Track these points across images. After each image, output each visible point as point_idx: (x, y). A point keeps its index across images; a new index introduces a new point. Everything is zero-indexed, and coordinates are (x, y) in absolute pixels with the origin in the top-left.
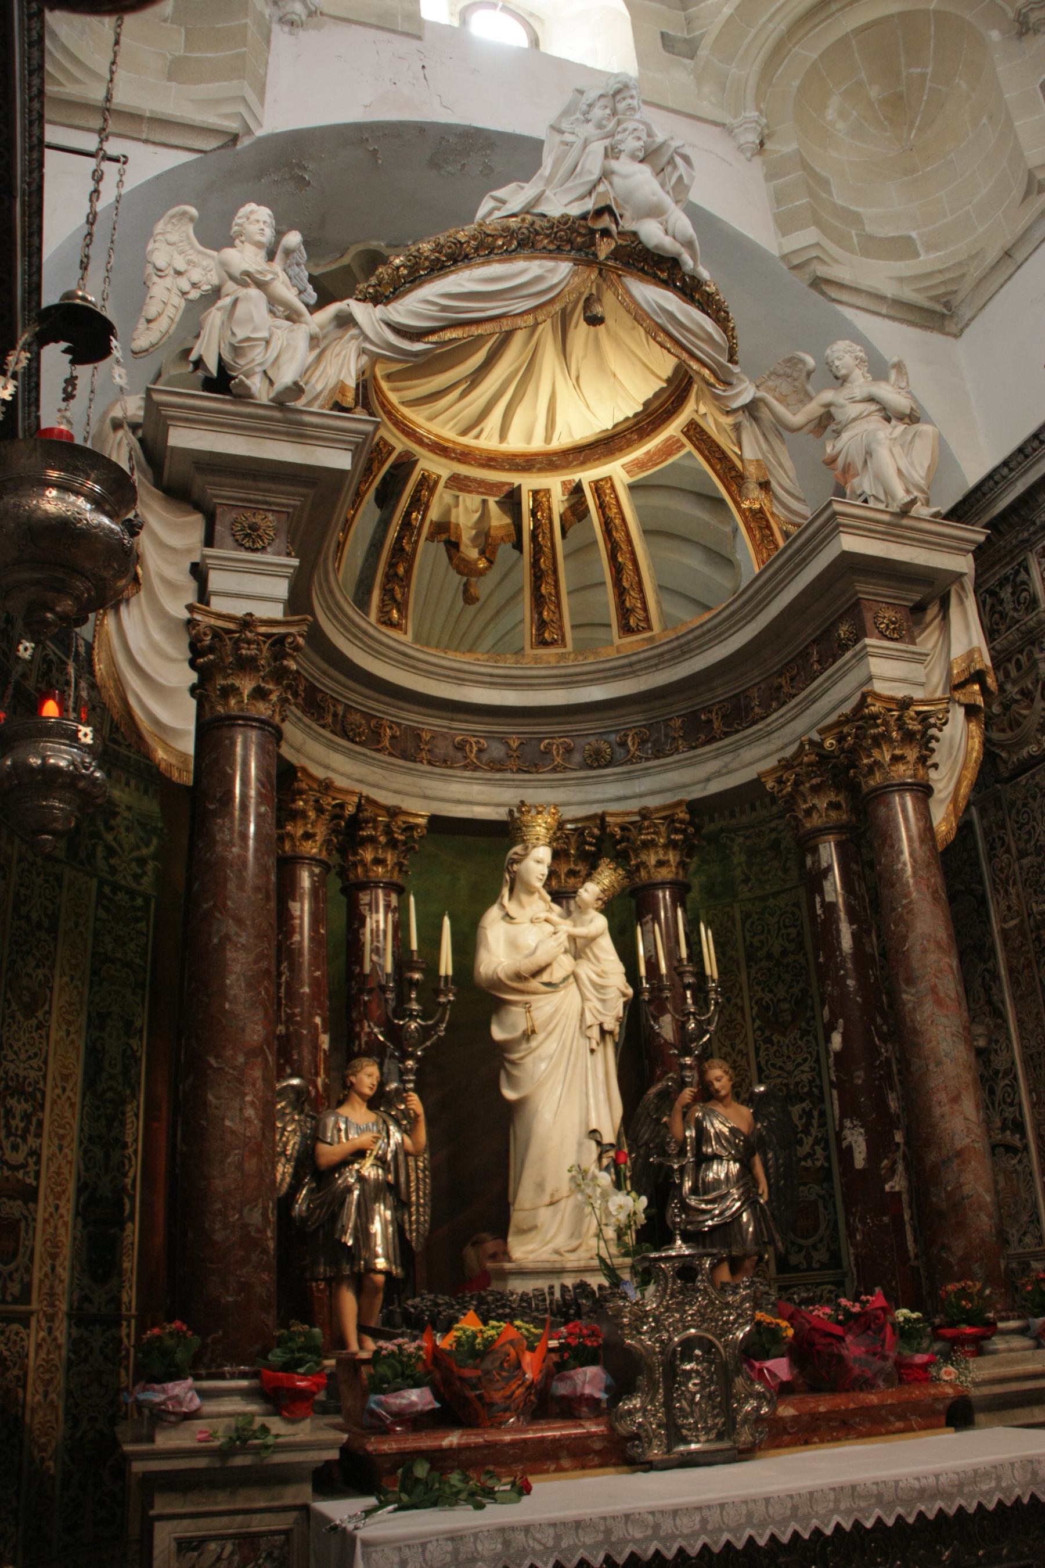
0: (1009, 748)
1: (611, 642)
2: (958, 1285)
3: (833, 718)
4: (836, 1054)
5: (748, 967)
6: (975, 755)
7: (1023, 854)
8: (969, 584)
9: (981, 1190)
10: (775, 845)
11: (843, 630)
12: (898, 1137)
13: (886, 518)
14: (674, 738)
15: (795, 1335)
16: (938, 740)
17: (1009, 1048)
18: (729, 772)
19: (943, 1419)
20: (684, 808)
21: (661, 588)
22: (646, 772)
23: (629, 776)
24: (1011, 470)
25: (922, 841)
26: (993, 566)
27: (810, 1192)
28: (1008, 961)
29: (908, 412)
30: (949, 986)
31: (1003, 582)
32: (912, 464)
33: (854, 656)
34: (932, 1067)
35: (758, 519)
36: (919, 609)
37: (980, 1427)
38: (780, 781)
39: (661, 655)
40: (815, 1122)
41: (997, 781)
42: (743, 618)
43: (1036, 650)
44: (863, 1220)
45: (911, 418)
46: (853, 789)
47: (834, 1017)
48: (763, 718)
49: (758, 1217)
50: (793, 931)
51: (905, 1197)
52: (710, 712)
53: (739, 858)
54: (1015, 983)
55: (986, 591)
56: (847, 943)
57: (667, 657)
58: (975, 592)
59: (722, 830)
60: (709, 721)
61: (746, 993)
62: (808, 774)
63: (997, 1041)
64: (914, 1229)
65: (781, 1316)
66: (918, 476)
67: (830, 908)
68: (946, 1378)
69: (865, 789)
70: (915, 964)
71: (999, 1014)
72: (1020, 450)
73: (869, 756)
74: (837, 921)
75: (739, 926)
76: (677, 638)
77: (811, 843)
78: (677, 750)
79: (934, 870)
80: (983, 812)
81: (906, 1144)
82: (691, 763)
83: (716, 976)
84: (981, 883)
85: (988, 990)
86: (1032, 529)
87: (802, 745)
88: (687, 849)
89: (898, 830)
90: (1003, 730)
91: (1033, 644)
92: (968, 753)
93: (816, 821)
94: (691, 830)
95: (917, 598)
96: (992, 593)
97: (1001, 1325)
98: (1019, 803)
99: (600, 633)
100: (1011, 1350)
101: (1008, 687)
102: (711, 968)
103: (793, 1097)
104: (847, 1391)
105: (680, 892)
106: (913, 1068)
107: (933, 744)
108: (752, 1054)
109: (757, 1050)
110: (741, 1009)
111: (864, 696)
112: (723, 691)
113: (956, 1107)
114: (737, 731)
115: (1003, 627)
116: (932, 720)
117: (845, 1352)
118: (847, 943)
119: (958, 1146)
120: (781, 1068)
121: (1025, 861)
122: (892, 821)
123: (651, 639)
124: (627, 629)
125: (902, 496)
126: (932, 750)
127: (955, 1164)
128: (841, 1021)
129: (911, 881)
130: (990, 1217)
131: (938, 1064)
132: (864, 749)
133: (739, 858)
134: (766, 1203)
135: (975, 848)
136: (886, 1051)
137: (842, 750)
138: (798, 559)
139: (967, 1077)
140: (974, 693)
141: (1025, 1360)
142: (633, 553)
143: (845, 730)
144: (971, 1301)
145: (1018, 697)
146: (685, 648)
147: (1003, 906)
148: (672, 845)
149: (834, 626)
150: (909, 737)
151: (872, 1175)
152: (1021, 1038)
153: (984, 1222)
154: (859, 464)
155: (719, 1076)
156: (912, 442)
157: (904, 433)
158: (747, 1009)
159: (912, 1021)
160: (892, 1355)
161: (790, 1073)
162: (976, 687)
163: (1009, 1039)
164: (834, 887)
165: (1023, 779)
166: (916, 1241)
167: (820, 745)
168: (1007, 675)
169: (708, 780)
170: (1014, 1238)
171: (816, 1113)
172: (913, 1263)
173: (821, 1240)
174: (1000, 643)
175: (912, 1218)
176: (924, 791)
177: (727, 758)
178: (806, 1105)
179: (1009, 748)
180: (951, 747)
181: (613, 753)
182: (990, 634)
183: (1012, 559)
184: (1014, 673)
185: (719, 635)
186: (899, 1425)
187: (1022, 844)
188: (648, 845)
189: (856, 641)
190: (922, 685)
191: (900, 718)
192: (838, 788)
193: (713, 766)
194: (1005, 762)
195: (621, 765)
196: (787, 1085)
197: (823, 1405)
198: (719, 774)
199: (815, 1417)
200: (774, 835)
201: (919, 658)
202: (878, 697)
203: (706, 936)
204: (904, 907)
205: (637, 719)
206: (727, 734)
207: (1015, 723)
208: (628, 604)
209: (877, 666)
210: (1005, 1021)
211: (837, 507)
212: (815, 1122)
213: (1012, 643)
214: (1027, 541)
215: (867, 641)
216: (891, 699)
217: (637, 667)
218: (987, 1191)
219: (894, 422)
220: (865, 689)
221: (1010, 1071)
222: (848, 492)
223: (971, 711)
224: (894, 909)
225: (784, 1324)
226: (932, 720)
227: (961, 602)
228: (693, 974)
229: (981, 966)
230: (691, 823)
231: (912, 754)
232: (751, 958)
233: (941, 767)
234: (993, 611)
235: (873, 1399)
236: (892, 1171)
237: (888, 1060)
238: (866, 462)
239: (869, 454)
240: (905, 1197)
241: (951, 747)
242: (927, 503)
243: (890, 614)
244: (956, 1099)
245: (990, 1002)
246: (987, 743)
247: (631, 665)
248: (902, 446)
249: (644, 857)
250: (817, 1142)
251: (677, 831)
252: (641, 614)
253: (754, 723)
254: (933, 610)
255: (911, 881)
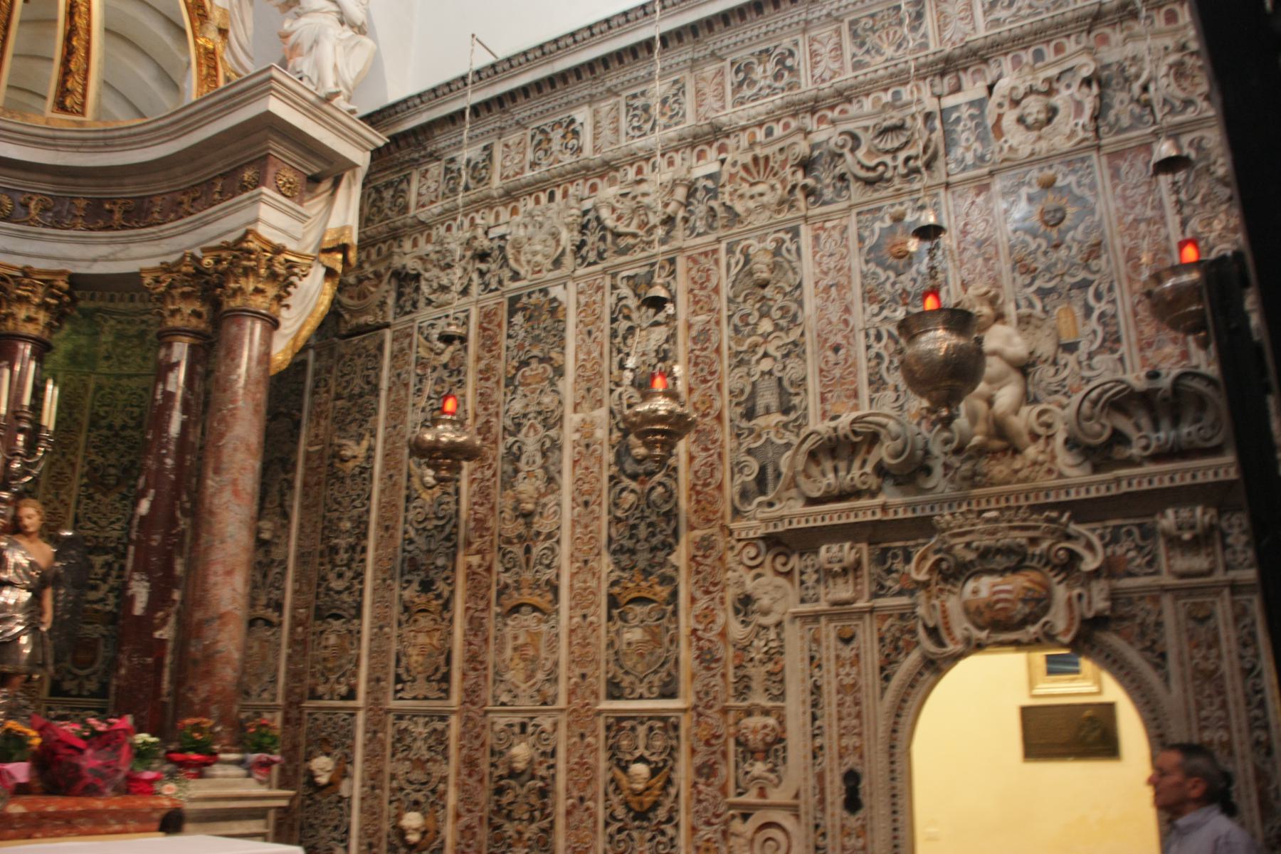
0: (353, 313)
1: (41, 113)
2: (196, 720)
3: (216, 243)
4: (142, 518)
5: (89, 431)
6: (322, 308)
7: (338, 397)
8: (361, 174)
9: (232, 648)
10: (142, 334)
11: (248, 175)
12: (177, 595)
13: (312, 98)
14: (75, 216)
15: (41, 745)
16: (296, 287)
17: (287, 545)
18: (115, 260)
19: (156, 825)
20: (65, 278)
21: (106, 84)
22: (40, 237)
23: (23, 235)
24: (422, 102)
25: (260, 362)
26: (386, 169)
27: (95, 631)
28: (305, 476)
29: (359, 23)
30: (248, 481)
31: (388, 185)
32: (347, 65)
33: (250, 198)
34: (217, 543)
35: (209, 56)
36: (315, 180)
37: (189, 833)
38: (157, 281)
39: (85, 140)
40: (114, 573)
41: (336, 336)
42: (168, 135)
43: (395, 244)
44: (129, 659)
45: (360, 29)
46: (216, 304)
47: (147, 486)
48: (159, 224)
49: (38, 640)
50: (137, 410)
51: (170, 646)
52: (115, 203)
53: (107, 338)
54: (305, 495)
55: (374, 187)
56: (174, 428)
57: (90, 143)
58: (364, 185)
59: (99, 310)
60: (111, 211)
61: (81, 453)
62: (183, 281)
63: (279, 537)
64: (172, 672)
65: (32, 727)
66: (349, 75)
67: (169, 396)
68: (167, 793)
69: (225, 308)
70: (225, 458)
71: (286, 515)
72: (434, 90)
73: (236, 282)
74: (171, 408)
75: (90, 394)
76: (105, 131)
77: (168, 339)
78: (73, 227)
79: (262, 388)
80: (318, 356)
81: (182, 602)
82: (84, 242)
83: (52, 427)
84: (300, 410)
85: (283, 495)
86: (423, 153)
87: (184, 256)
88: (60, 315)
89: (241, 346)
90: (351, 298)
91: (395, 239)
92: (317, 305)
93: (177, 322)
94: (67, 299)
95: (316, 170)
96: (378, 190)
97: (223, 756)
98: (348, 357)
99: (37, 103)
100: (226, 776)
101: (366, 266)
102: (49, 418)
103: (98, 549)
104: (78, 795)
105: (42, 350)
106: (202, 541)
107: (291, 289)
108: (73, 505)
109: (79, 502)
110: (73, 465)
111: (248, 232)
112: (130, 190)
113: (228, 579)
114: (133, 228)
115: (377, 219)
116: (296, 270)
117: (84, 763)
118: (174, 428)
119: (223, 609)
120: (95, 523)
121: (339, 403)
122: (238, 339)
123: (81, 123)
124: (61, 107)
125: (330, 87)
126: (289, 294)
127: (216, 624)
128: (152, 491)
129: (241, 392)
130: (235, 671)
131: (223, 542)
132: (235, 275)
133: (107, 338)
134: (50, 631)
135: (303, 383)
136: (184, 523)
137: (216, 271)
138: (229, 103)
139: (244, 557)
140: (336, 260)
141: (235, 785)
142: (88, 42)
143: (224, 254)
144: (202, 734)
145: (371, 276)
146: (109, 142)
147: (313, 432)
148: (44, 306)
149: (241, 168)
150: (273, 276)
151: (146, 623)
152: (299, 539)
153: (228, 674)
154: (306, 47)
155: (31, 515)
156: (353, 47)
157: (350, 39)
158: (78, 467)
159: (211, 503)
160: (125, 769)
161: (102, 528)
162: (340, 256)
163: (288, 536)
164: (178, 380)
165: (355, 339)
166: (171, 682)
167: (199, 261)
168: (368, 256)
169: (95, 260)
170: (255, 688)
171: (116, 566)
172: (165, 699)
173: (94, 673)
174: (371, 230)
175: (172, 663)
176: (273, 324)
177: (117, 248)
178: (110, 558)
179: (353, 313)
180: (305, 296)
181: (13, 210)
182: (365, 220)
183: (401, 170)
184: (374, 257)
185: (142, 142)
186: (117, 827)
187: (340, 389)
188: (21, 299)
189: (255, 187)
190: (297, 240)
191: (270, 260)
192: (204, 300)
193: (103, 250)
194: (346, 322)
195: (17, 223)
196: (96, 537)
197: (52, 805)
198: (106, 259)
199: (43, 816)
200: (143, 327)
201: (302, 218)
202: (258, 237)
203: (51, 391)
204: (230, 410)
205: (46, 187)
206: (123, 227)
207: (363, 295)
208: (69, 85)
209: (265, 212)
210: (290, 522)
211: (275, 73)
212: (114, 573)
213: (380, 233)
214: (416, 160)
215: (264, 189)
216: (268, 242)
217: (60, 142)
218: (237, 650)
219: (346, 27)
220: (250, 227)
221: (283, 563)
222: (290, 66)
223: (330, 273)
224: (220, 410)
225: (33, 733)
226: (296, 270)
227: (350, 186)
228: (30, 421)
229: (282, 476)
230: (69, 293)
231: (272, 291)
232: (94, 424)
233: (292, 310)
234: (373, 204)
235: (99, 804)
236: (164, 622)
237: (184, 531)
238: (311, 48)
239: (316, 42)
240: (170, 646)
241: (305, 296)
242: (349, 100)
243: (290, 175)
244: (229, 573)
245: (281, 505)
246: (335, 302)
247: (54, 138)
248: (344, 48)
249: (15, 309)
250: (112, 590)
251: (53, 296)
252: (78, 99)
253: (150, 225)
254: (326, 185)
255: (241, 392)
